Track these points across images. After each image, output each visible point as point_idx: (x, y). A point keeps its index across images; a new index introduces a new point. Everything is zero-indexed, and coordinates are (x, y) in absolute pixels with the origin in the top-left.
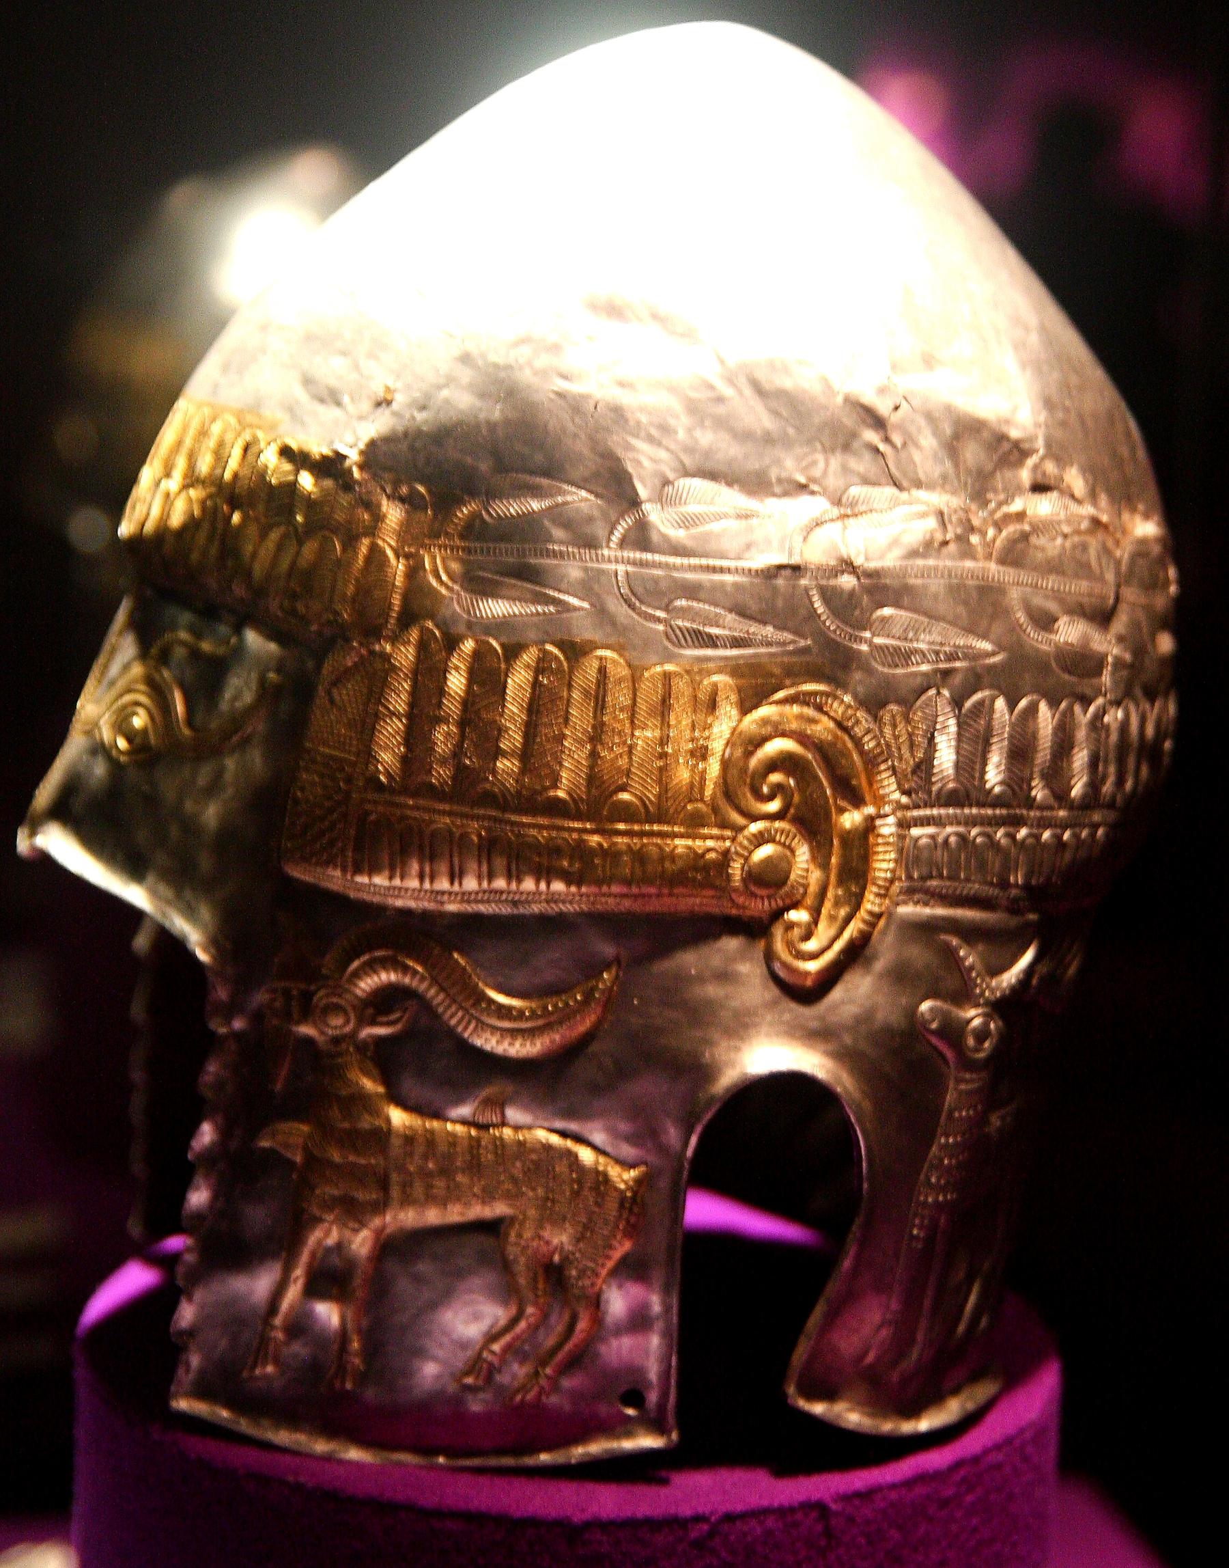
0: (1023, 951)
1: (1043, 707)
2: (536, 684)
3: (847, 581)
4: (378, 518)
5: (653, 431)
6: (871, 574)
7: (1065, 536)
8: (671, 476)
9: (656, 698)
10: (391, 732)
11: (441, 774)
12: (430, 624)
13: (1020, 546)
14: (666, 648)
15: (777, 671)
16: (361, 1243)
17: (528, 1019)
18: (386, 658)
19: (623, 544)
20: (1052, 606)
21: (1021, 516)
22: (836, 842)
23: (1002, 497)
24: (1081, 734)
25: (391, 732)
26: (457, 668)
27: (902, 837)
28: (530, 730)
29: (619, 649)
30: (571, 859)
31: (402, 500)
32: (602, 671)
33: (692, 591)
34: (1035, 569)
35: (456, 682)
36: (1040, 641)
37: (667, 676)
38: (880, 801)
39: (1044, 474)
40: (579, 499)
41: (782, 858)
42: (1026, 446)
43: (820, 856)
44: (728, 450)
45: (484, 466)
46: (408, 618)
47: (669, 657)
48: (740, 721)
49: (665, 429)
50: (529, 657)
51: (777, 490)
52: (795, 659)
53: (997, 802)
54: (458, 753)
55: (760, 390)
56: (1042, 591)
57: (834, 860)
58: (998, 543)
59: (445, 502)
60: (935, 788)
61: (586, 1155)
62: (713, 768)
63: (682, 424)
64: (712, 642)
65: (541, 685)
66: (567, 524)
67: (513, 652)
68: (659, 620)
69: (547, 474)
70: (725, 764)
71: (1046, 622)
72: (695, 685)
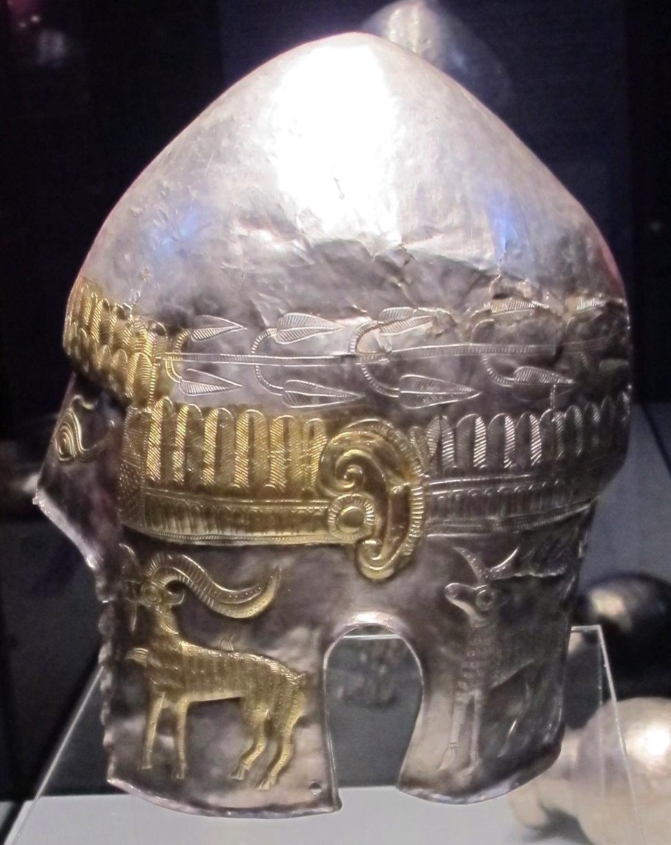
0: (514, 550)
1: (508, 419)
2: (219, 428)
3: (384, 361)
4: (144, 342)
5: (272, 288)
6: (399, 355)
7: (518, 322)
8: (282, 311)
9: (280, 433)
10: (153, 455)
11: (179, 477)
12: (167, 398)
13: (488, 331)
14: (284, 406)
15: (347, 412)
16: (182, 706)
17: (237, 599)
18: (149, 415)
19: (258, 351)
20: (512, 363)
21: (488, 312)
22: (390, 502)
23: (475, 304)
24: (536, 431)
25: (153, 455)
26: (181, 422)
27: (426, 497)
28: (218, 452)
29: (260, 408)
30: (245, 519)
31: (154, 331)
32: (251, 420)
33: (297, 374)
34: (498, 342)
35: (181, 430)
36: (505, 383)
37: (286, 421)
38: (413, 477)
39: (502, 287)
40: (236, 328)
41: (358, 512)
42: (489, 274)
43: (382, 510)
44: (314, 294)
45: (190, 312)
46: (158, 395)
47: (285, 410)
48: (328, 442)
49: (278, 286)
50: (215, 413)
51: (343, 313)
52: (357, 406)
53: (484, 472)
54: (185, 466)
55: (329, 260)
56: (503, 354)
57: (389, 511)
58: (473, 331)
59: (173, 331)
60: (444, 469)
61: (274, 666)
62: (315, 468)
63: (287, 283)
64: (308, 400)
65: (222, 429)
66: (230, 342)
67: (206, 411)
68: (278, 391)
69: (218, 314)
70: (321, 465)
71: (509, 371)
72: (301, 424)
